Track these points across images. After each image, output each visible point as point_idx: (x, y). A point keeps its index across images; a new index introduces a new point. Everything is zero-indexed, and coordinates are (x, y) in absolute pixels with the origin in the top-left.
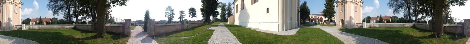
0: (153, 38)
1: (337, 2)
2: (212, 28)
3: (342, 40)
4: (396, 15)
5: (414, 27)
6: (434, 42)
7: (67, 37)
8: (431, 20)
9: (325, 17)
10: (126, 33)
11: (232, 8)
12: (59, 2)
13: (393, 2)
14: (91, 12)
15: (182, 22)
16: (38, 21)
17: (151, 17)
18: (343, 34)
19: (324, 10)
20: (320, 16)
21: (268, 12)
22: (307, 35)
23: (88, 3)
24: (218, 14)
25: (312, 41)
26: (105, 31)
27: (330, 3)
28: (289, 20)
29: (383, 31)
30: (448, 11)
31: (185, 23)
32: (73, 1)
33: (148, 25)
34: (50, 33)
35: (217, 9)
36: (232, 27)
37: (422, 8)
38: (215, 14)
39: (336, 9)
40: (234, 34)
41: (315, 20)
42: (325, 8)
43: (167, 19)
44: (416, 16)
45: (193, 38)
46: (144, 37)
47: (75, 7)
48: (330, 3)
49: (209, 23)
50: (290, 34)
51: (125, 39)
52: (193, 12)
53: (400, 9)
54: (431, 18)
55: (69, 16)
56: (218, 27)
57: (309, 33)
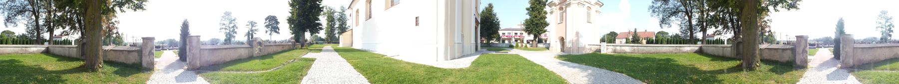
0: (198, 73)
1: (551, 5)
2: (310, 55)
3: (564, 76)
4: (665, 29)
5: (47, 52)
6: (744, 79)
7: (29, 68)
9: (529, 34)
11: (348, 16)
13: (659, 4)
14: (732, 21)
15: (251, 41)
16: (631, 38)
17: (847, 30)
18: (564, 64)
19: (526, 21)
20: (519, 32)
22: (493, 69)
24: (321, 29)
25: (503, 80)
26: (758, 58)
28: (457, 39)
29: (638, 58)
30: (113, 21)
31: (255, 43)
33: (841, 45)
34: (653, 60)
35: (318, 19)
36: (347, 52)
39: (549, 19)
40: (356, 67)
41: (509, 40)
42: (528, 17)
43: (222, 37)
44: (704, 30)
47: (702, 12)
49: (302, 46)
50: (458, 67)
51: (142, 75)
52: (273, 24)
53: (673, 18)
54: (733, 32)
57: (498, 65)
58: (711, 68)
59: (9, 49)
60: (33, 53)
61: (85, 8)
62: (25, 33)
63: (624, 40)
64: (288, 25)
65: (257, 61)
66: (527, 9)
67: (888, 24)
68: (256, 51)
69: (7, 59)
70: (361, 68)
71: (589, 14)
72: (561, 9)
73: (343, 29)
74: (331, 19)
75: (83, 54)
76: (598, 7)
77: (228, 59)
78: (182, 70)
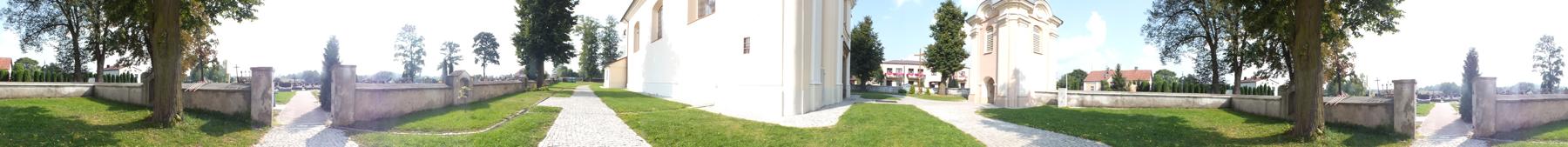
0: (348, 135)
2: (552, 102)
4: (1170, 65)
5: (1229, 107)
7: (62, 121)
8: (153, 70)
10: (1398, 128)
11: (620, 34)
12: (44, 5)
13: (21, 7)
15: (451, 77)
16: (1110, 80)
17: (344, 58)
18: (991, 124)
21: (746, 50)
23: (128, 10)
24: (573, 55)
26: (1321, 120)
27: (951, 24)
28: (815, 78)
29: (1124, 116)
30: (208, 39)
31: (457, 81)
32: (90, 5)
33: (333, 86)
34: (1149, 119)
35: (568, 38)
37: (118, 33)
38: (561, 53)
39: (970, 45)
40: (633, 124)
41: (899, 80)
42: (933, 42)
43: (398, 70)
45: (484, 136)
46: (320, 128)
48: (951, 24)
50: (820, 125)
51: (248, 134)
52: (487, 46)
53: (1184, 47)
54: (1287, 75)
55: (76, 53)
56: (573, 98)
58: (1244, 135)
59: (29, 90)
60: (68, 96)
61: (152, 18)
62: (55, 62)
63: (1098, 85)
64: (515, 49)
65: (461, 113)
66: (932, 28)
67: (415, 49)
68: (459, 94)
69: (24, 106)
70: (648, 132)
71: (1036, 39)
72: (990, 28)
73: (611, 57)
74: (590, 39)
75: (1291, 111)
76: (1053, 26)
77: (408, 110)
78: (1465, 139)
